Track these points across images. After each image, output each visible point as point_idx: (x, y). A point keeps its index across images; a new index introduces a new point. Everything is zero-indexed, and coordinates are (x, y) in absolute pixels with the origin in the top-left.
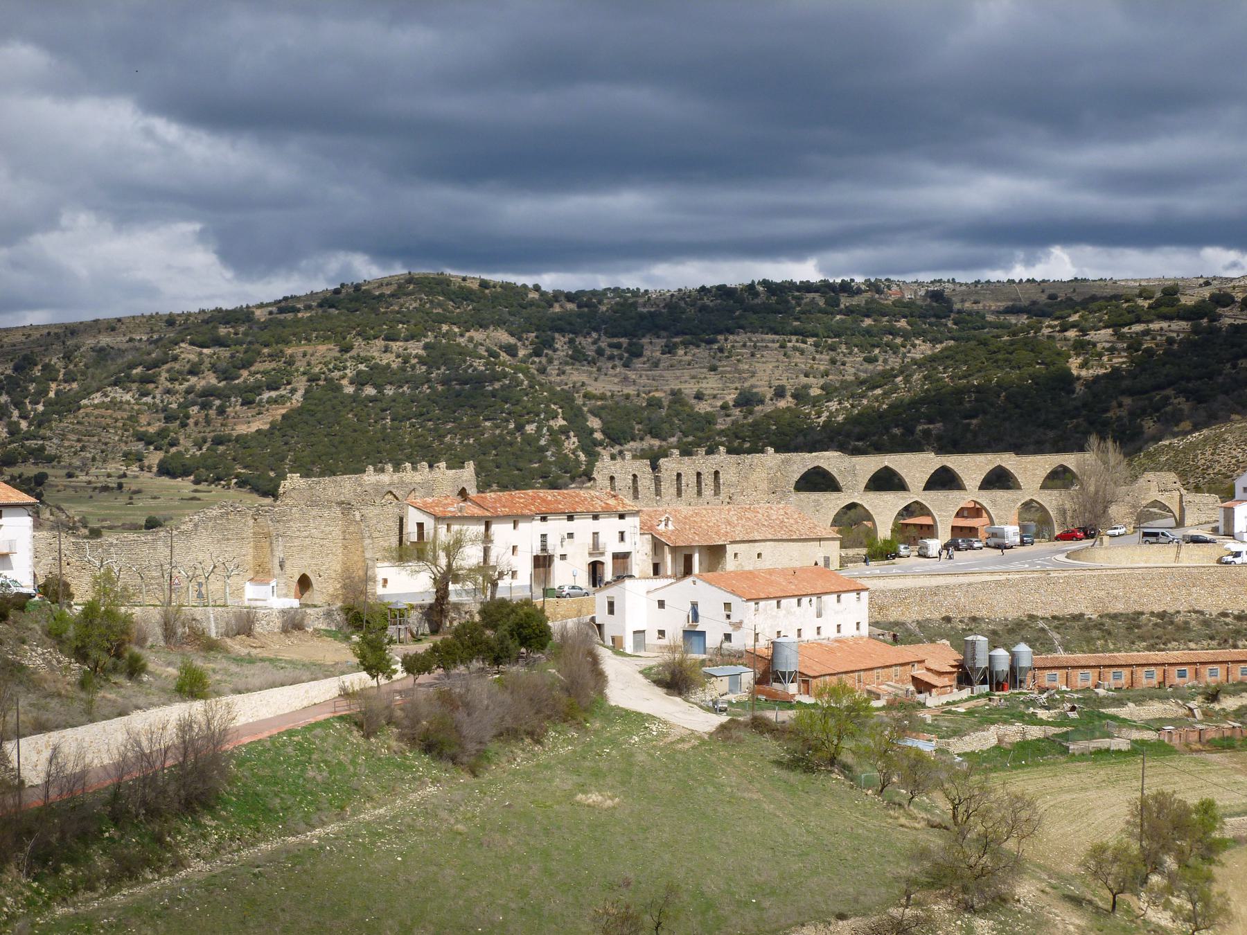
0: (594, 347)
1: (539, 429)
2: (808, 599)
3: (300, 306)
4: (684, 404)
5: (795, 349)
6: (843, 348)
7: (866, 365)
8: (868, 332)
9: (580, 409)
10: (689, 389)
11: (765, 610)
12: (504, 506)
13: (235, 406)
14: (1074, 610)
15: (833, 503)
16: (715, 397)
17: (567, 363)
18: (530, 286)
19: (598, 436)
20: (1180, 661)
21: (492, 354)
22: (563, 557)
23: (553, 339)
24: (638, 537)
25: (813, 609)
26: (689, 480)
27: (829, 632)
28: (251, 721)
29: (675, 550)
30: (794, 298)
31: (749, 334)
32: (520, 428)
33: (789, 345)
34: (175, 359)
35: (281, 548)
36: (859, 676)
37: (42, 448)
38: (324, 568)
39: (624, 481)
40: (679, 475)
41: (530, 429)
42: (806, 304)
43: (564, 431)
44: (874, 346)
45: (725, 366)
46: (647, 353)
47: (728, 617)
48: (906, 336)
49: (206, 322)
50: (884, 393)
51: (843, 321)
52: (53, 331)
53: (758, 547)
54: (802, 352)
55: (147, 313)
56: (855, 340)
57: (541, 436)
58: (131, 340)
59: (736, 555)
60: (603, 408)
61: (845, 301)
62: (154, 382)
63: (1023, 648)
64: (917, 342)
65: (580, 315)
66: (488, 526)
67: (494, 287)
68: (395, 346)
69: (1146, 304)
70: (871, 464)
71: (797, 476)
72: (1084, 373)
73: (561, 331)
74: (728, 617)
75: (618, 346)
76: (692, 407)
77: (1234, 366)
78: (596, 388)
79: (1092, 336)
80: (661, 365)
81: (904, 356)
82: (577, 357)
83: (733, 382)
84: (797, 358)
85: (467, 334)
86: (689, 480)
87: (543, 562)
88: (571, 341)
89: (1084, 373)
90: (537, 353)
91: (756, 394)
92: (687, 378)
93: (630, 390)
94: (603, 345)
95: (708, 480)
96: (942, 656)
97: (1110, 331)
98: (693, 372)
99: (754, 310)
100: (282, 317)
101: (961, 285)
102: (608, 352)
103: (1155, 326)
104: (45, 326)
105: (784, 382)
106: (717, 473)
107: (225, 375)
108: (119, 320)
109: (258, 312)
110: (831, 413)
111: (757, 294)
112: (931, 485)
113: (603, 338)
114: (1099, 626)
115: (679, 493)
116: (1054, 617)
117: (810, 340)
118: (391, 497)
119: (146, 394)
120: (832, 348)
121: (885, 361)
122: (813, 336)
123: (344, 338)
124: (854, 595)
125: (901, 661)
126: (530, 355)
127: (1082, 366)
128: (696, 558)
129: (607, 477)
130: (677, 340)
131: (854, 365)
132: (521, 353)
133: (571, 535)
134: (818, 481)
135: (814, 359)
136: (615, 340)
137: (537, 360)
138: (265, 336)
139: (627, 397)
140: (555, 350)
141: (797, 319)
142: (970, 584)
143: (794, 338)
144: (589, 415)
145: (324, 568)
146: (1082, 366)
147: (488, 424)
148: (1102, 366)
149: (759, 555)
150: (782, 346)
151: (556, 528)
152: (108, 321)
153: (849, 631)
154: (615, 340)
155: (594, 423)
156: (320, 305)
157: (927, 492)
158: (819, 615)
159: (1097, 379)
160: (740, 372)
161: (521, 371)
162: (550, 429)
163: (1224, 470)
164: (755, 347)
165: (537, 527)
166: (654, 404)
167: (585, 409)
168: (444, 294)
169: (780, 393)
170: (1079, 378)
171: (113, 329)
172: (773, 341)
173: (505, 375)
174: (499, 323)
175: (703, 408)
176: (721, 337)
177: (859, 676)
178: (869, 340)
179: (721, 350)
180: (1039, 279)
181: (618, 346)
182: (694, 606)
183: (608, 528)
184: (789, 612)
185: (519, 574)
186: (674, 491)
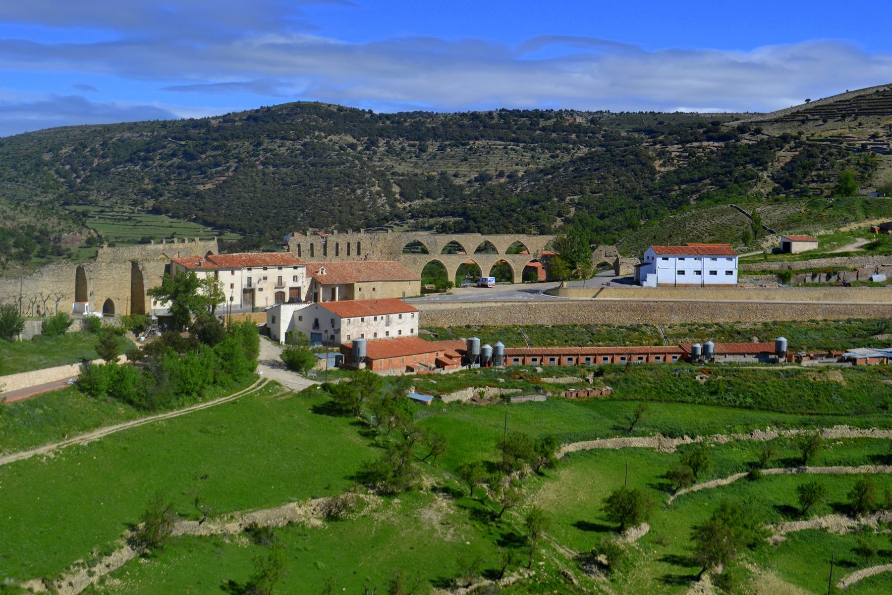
0: (400, 146)
1: (365, 192)
2: (381, 316)
3: (237, 119)
4: (446, 179)
5: (512, 149)
6: (539, 150)
7: (552, 160)
8: (554, 141)
9: (388, 181)
10: (451, 171)
11: (354, 323)
12: (226, 262)
13: (196, 176)
14: (540, 322)
15: (423, 261)
16: (465, 176)
17: (384, 155)
18: (367, 111)
19: (397, 196)
20: (588, 353)
21: (341, 148)
22: (261, 290)
23: (378, 141)
24: (305, 278)
25: (384, 322)
26: (343, 247)
27: (394, 334)
28: (29, 386)
29: (324, 286)
30: (514, 120)
31: (487, 141)
32: (353, 191)
33: (510, 147)
34: (164, 147)
35: (92, 286)
36: (403, 359)
37: (87, 196)
38: (121, 295)
39: (305, 247)
40: (337, 244)
41: (359, 192)
42: (520, 124)
43: (378, 193)
44: (556, 148)
45: (473, 159)
46: (430, 150)
47: (333, 326)
48: (574, 143)
49: (184, 126)
50: (553, 178)
51: (540, 135)
52: (98, 129)
53: (373, 285)
54: (516, 151)
55: (152, 120)
56: (546, 145)
57: (364, 197)
58: (141, 135)
59: (360, 289)
60: (402, 180)
61: (542, 123)
62: (152, 160)
63: (501, 345)
64: (581, 147)
65: (393, 128)
66: (216, 273)
67: (346, 110)
68: (288, 143)
69: (701, 131)
70: (445, 239)
71: (404, 245)
72: (663, 169)
73: (381, 136)
74: (333, 326)
75: (413, 146)
76: (452, 181)
77: (744, 168)
78: (399, 169)
79: (670, 148)
80: (437, 157)
81: (573, 155)
82: (390, 151)
83: (477, 168)
84: (513, 155)
85: (330, 137)
86: (343, 247)
87: (249, 292)
88: (388, 143)
89: (663, 169)
90: (367, 148)
91: (488, 174)
92: (450, 165)
93: (419, 171)
94: (406, 145)
95: (354, 248)
96: (451, 348)
97: (680, 146)
98: (455, 162)
99: (492, 127)
100: (226, 124)
101: (612, 114)
102: (408, 149)
103: (705, 144)
104: (94, 126)
105: (504, 169)
106: (359, 243)
107: (188, 156)
108: (135, 123)
109: (213, 122)
110: (523, 188)
111: (493, 118)
112: (479, 250)
113: (406, 141)
114: (551, 332)
115: (337, 254)
116: (527, 327)
117: (521, 145)
118: (164, 256)
119: (147, 167)
120: (533, 149)
121: (562, 158)
122: (523, 142)
123: (260, 138)
124: (410, 314)
125: (430, 351)
126: (364, 149)
127: (661, 165)
128: (337, 288)
129: (296, 245)
130: (447, 143)
131: (544, 160)
132: (360, 148)
133: (265, 278)
134: (415, 248)
135: (522, 156)
136: (412, 142)
137: (368, 152)
138: (215, 135)
139: (416, 175)
140: (378, 147)
141: (514, 133)
142: (483, 308)
143: (512, 143)
144: (394, 184)
145: (121, 295)
146: (661, 165)
147: (336, 188)
148: (673, 165)
149: (374, 289)
150: (505, 148)
151: (256, 273)
152: (129, 124)
153: (406, 333)
154: (412, 142)
155: (396, 189)
156: (248, 119)
157: (476, 255)
158: (387, 324)
159: (668, 172)
160: (480, 162)
161: (357, 158)
162: (371, 192)
163: (698, 233)
164: (490, 147)
165: (245, 273)
166: (430, 179)
167: (392, 181)
168: (317, 115)
169: (501, 174)
170: (659, 172)
171: (132, 129)
172: (500, 145)
173: (348, 161)
174: (346, 132)
175: (458, 182)
176: (471, 142)
177: (403, 359)
178: (551, 146)
179: (470, 149)
180: (656, 112)
181: (413, 146)
182: (316, 321)
183: (287, 274)
184: (368, 324)
185: (235, 299)
186: (334, 252)
